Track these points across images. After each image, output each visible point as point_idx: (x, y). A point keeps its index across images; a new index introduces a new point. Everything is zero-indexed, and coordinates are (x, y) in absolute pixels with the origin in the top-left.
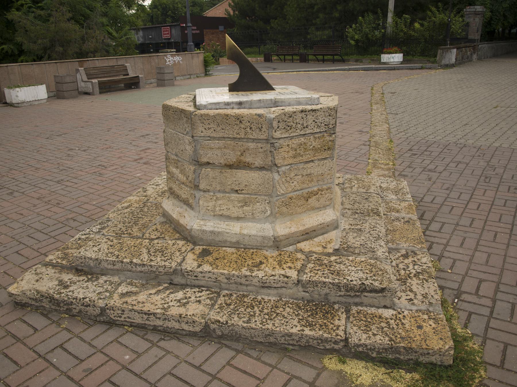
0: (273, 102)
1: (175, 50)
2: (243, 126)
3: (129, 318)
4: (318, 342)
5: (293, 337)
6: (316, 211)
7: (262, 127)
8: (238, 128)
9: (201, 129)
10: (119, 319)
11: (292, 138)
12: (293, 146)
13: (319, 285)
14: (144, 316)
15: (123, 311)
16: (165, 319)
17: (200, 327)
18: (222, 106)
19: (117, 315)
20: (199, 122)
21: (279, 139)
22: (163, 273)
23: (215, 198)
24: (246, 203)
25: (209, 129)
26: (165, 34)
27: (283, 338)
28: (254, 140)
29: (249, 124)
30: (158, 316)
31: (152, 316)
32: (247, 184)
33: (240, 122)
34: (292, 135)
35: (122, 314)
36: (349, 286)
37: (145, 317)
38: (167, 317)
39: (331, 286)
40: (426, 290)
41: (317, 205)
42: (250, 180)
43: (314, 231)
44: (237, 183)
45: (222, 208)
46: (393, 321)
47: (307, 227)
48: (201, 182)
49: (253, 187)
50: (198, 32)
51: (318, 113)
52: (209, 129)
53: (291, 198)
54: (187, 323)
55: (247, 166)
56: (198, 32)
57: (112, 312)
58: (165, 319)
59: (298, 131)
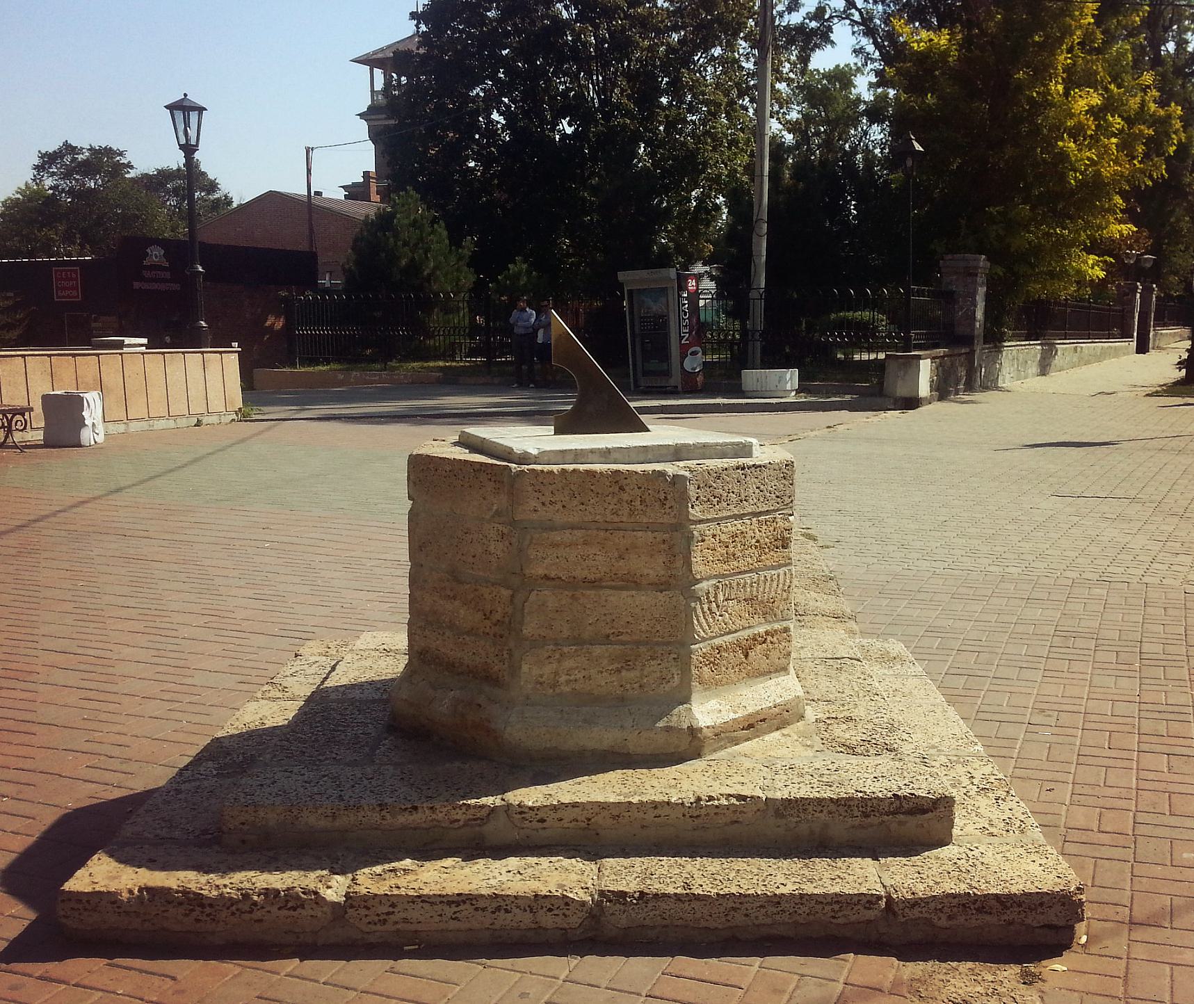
0: (672, 450)
1: (144, 341)
2: (625, 497)
3: (405, 920)
4: (833, 910)
5: (784, 905)
6: (761, 679)
7: (666, 499)
8: (615, 500)
9: (533, 503)
10: (379, 927)
11: (718, 521)
12: (723, 537)
13: (810, 808)
14: (446, 908)
15: (393, 905)
16: (498, 909)
17: (580, 914)
18: (614, 455)
19: (376, 918)
20: (530, 489)
21: (701, 521)
22: (461, 823)
23: (557, 656)
24: (627, 662)
25: (551, 503)
26: (65, 288)
27: (763, 911)
28: (647, 528)
29: (639, 492)
30: (481, 904)
31: (467, 906)
32: (630, 619)
33: (622, 488)
34: (720, 515)
35: (388, 914)
36: (869, 804)
37: (449, 911)
38: (503, 904)
39: (833, 807)
40: (1008, 814)
41: (764, 664)
42: (637, 610)
43: (764, 720)
44: (608, 619)
45: (572, 678)
46: (963, 861)
47: (751, 710)
48: (527, 619)
49: (643, 627)
50: (177, 287)
51: (766, 473)
52: (551, 503)
53: (719, 648)
54: (550, 910)
55: (632, 583)
56: (177, 287)
57: (363, 912)
58: (498, 909)
59: (731, 507)
